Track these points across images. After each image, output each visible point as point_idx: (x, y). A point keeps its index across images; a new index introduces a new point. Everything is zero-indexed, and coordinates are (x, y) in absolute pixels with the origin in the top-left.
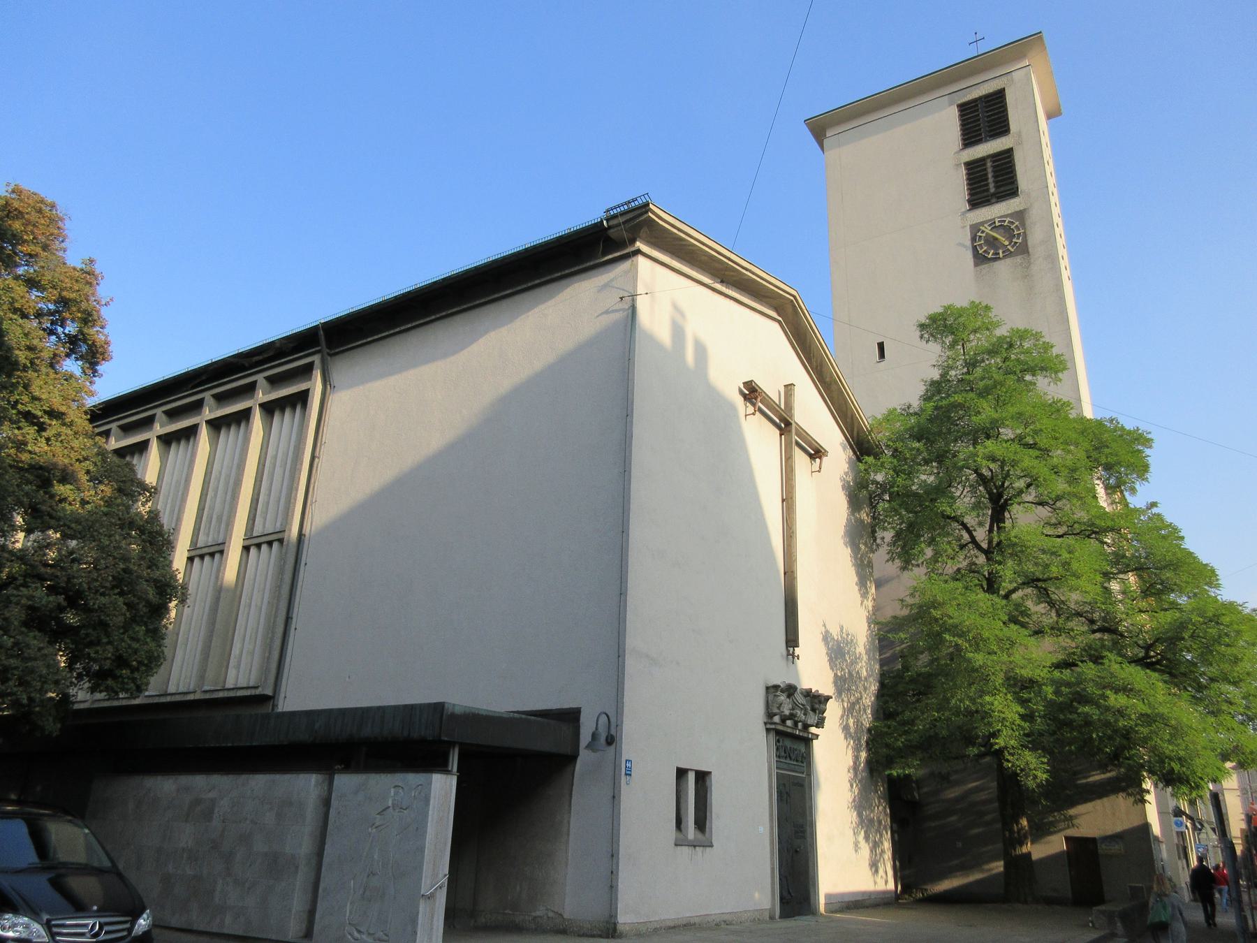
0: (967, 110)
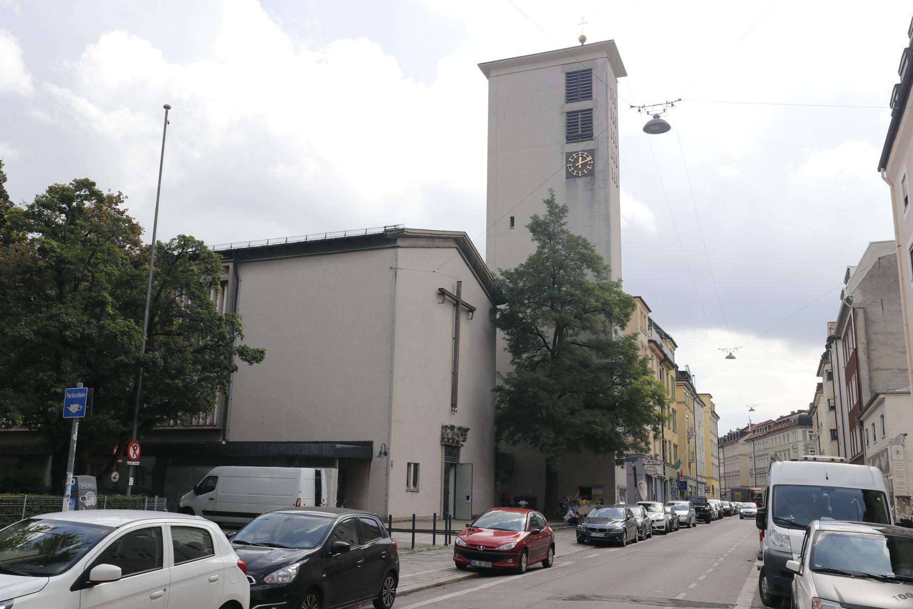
0: (571, 77)
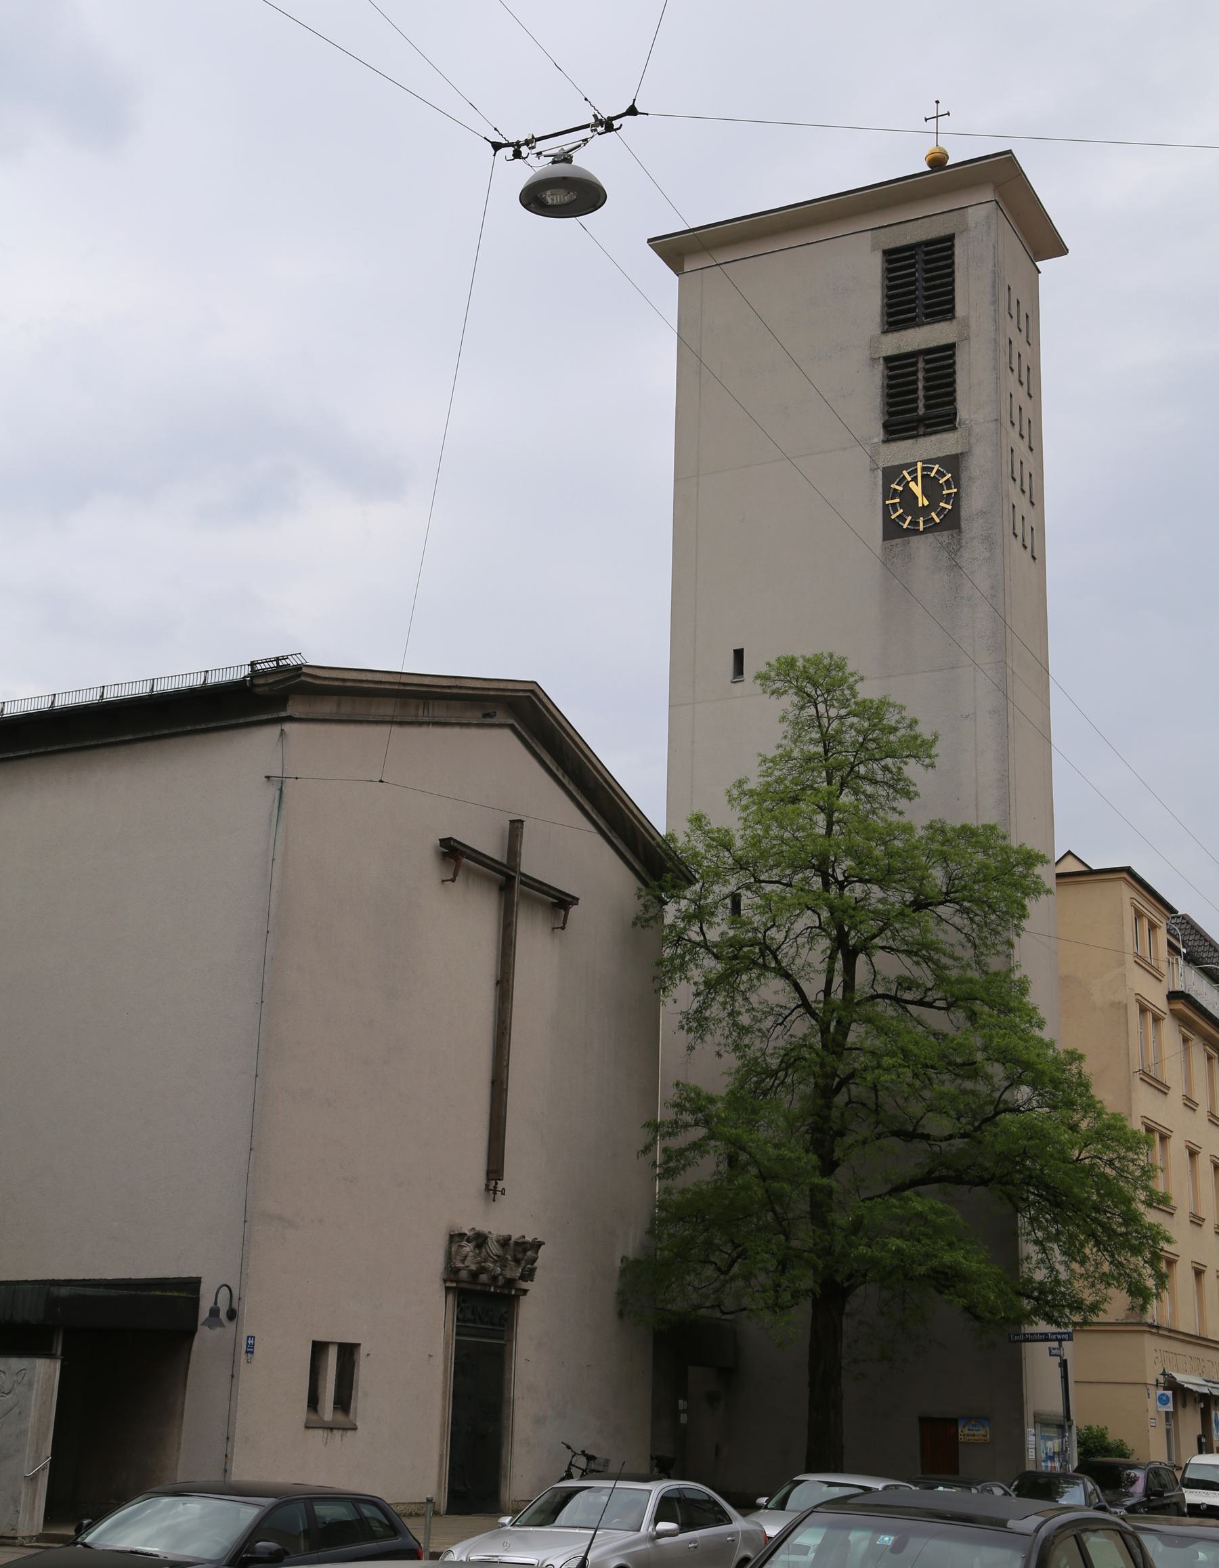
0: (895, 259)
